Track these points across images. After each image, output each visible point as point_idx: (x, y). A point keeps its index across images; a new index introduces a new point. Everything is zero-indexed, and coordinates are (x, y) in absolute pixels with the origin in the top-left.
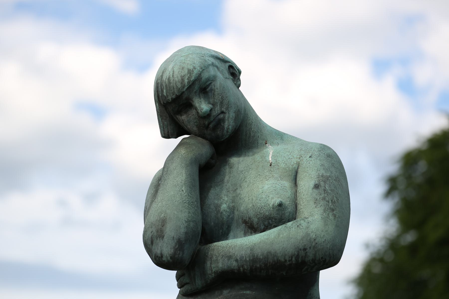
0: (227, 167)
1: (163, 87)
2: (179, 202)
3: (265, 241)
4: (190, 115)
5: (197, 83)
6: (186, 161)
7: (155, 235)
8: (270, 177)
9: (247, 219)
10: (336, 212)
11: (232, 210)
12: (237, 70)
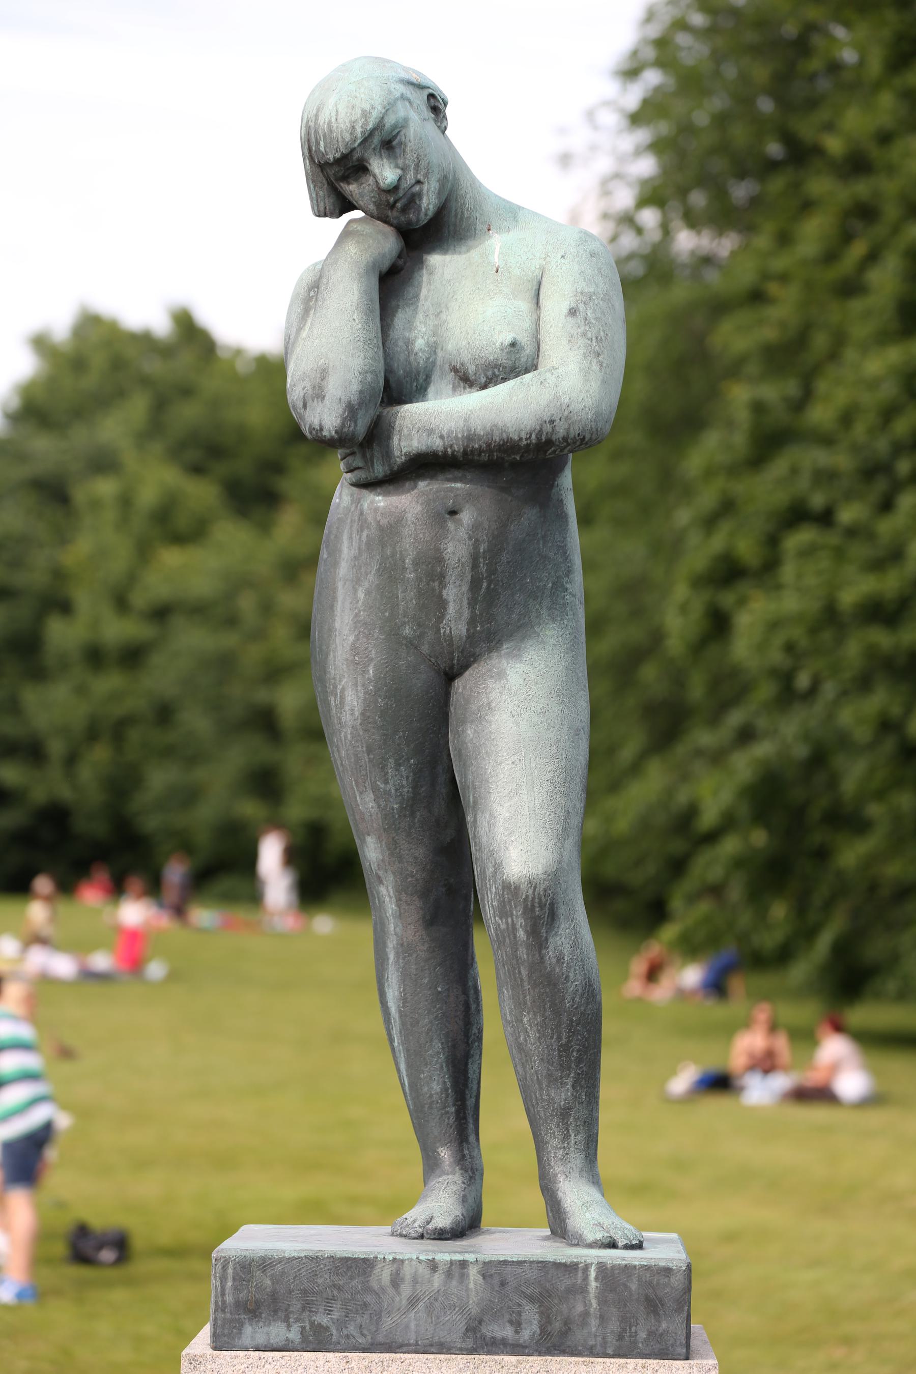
0: (425, 271)
3: (488, 406)
4: (364, 185)
5: (376, 133)
7: (311, 393)
8: (496, 294)
9: (458, 365)
10: (603, 358)
11: (434, 349)
12: (441, 101)
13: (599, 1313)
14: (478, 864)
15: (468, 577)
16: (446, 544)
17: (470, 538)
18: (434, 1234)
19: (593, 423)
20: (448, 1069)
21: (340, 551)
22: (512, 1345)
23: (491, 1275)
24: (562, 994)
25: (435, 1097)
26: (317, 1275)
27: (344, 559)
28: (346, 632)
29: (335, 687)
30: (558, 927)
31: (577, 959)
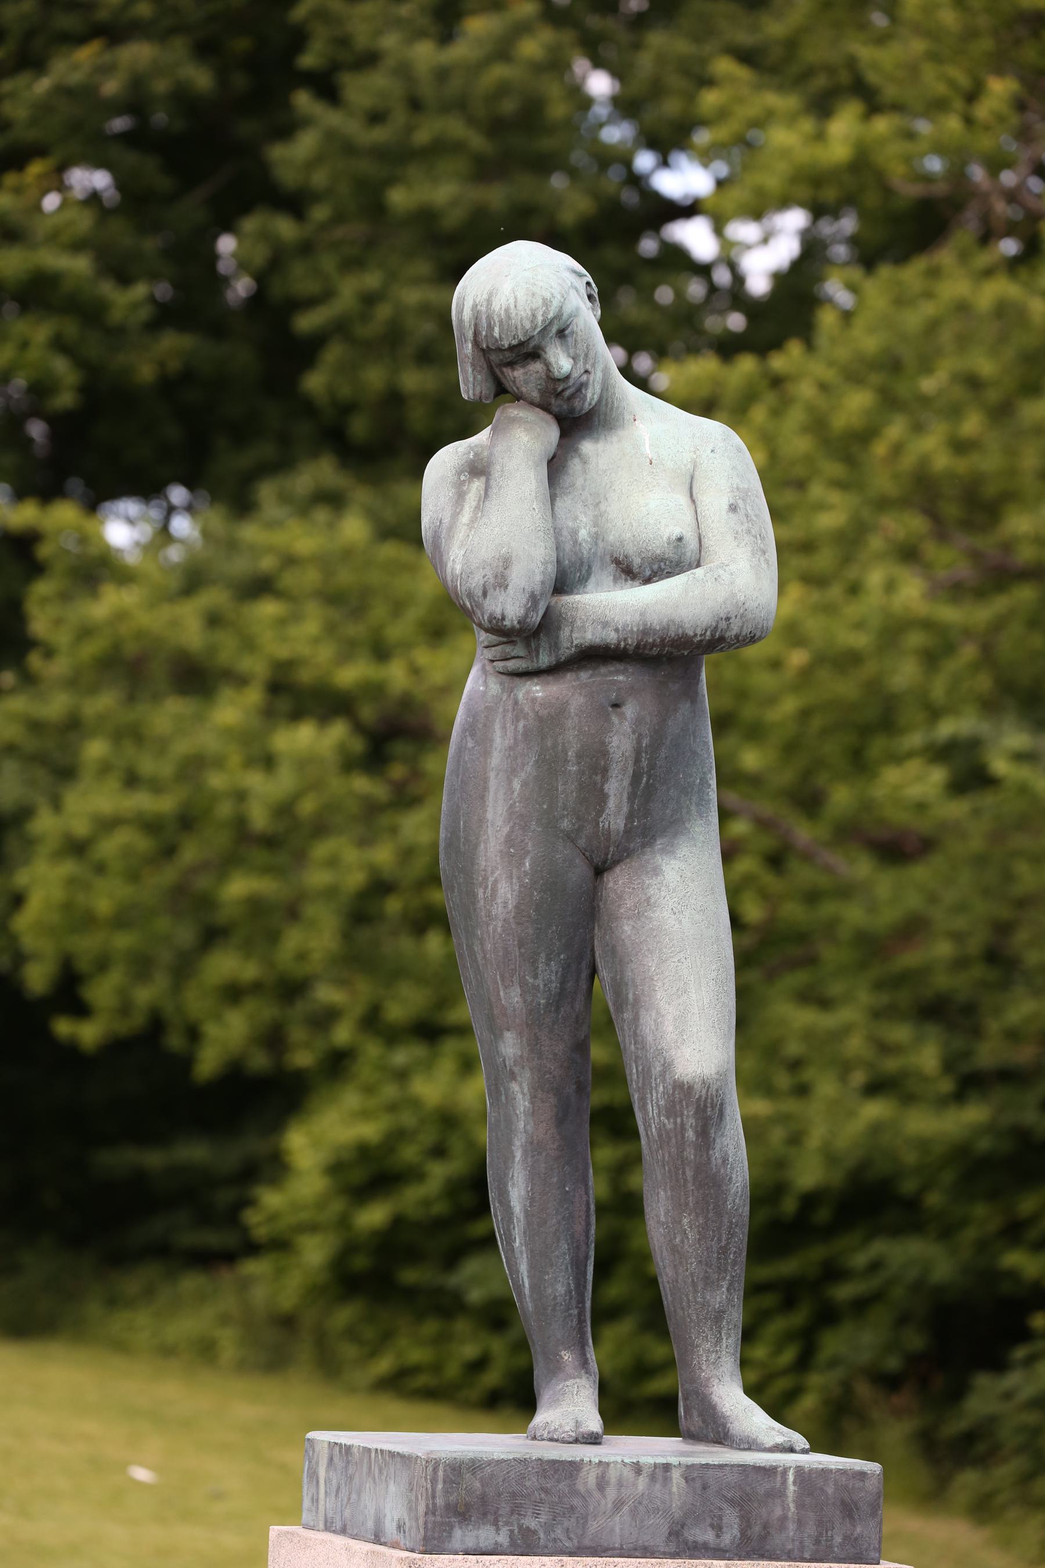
1: (492, 323)
2: (530, 529)
5: (555, 322)
6: (534, 457)
13: (796, 1517)
14: (640, 1063)
15: (630, 770)
16: (611, 737)
17: (634, 732)
18: (591, 1439)
19: (765, 621)
20: (573, 1271)
21: (492, 741)
22: (714, 1549)
23: (693, 1479)
24: (725, 1196)
25: (559, 1299)
26: (525, 1478)
27: (496, 749)
28: (500, 823)
29: (486, 878)
30: (725, 1128)
31: (738, 1160)
